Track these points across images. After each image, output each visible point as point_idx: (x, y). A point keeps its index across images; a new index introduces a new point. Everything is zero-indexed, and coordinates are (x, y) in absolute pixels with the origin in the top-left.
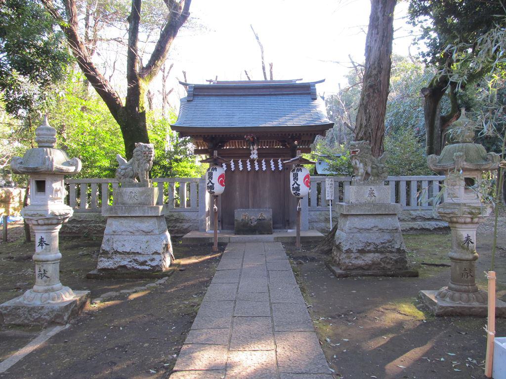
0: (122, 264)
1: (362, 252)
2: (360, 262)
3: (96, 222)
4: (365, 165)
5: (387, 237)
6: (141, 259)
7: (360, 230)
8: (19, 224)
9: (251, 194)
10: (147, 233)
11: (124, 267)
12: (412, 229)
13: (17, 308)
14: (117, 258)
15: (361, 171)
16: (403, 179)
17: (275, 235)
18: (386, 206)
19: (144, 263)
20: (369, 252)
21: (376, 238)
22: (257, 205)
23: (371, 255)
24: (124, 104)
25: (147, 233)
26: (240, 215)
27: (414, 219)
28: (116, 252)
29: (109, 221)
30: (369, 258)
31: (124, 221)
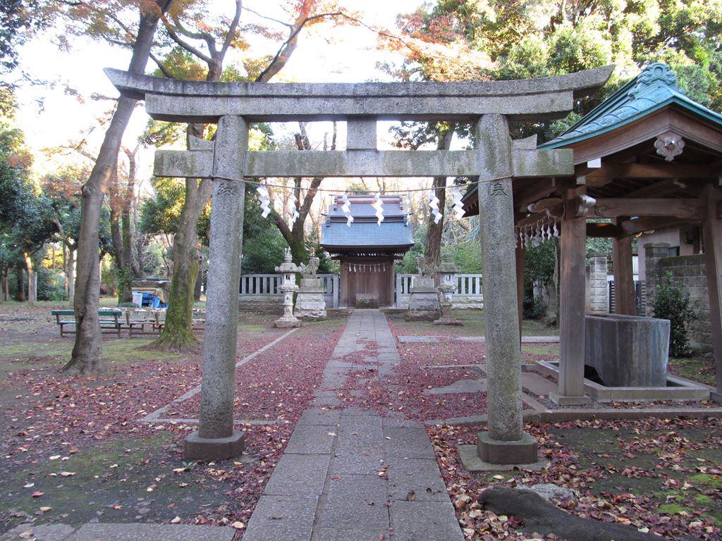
0: (306, 314)
1: (418, 310)
2: (418, 315)
3: (266, 302)
4: (422, 269)
5: (431, 303)
6: (314, 312)
7: (418, 300)
8: (30, 337)
9: (366, 284)
10: (317, 301)
11: (307, 316)
12: (469, 308)
13: (281, 322)
14: (303, 312)
15: (421, 272)
16: (464, 276)
17: (380, 308)
18: (432, 289)
19: (316, 315)
20: (422, 310)
21: (425, 304)
22: (369, 291)
23: (423, 312)
24: (291, 228)
25: (317, 301)
26: (360, 297)
27: (470, 302)
28: (303, 310)
29: (299, 295)
30: (422, 313)
31: (306, 295)
